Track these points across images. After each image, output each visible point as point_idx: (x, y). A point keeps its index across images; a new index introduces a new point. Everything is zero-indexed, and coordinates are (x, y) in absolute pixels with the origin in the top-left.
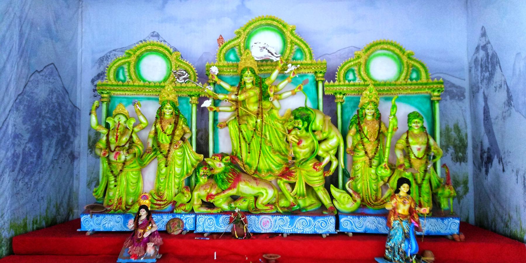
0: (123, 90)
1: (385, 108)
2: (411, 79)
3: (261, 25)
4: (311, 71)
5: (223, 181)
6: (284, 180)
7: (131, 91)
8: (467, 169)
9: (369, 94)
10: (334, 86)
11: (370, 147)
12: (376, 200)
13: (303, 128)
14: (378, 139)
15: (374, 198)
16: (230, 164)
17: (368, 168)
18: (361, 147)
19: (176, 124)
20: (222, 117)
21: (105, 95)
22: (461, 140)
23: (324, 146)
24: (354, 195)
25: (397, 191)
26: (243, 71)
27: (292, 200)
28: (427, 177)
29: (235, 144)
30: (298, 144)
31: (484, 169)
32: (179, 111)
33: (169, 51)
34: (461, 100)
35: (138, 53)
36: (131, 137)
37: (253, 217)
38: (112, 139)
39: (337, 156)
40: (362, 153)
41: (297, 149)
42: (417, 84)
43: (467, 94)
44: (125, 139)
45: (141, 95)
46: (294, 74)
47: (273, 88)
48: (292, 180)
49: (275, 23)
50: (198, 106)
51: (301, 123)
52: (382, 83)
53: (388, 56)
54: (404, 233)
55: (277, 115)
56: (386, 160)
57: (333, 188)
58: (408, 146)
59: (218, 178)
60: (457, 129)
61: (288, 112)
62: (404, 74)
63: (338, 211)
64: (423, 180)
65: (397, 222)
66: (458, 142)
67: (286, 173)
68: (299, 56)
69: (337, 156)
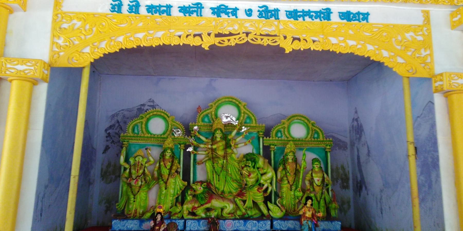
0: (137, 140)
1: (300, 155)
2: (314, 138)
3: (225, 101)
4: (256, 130)
5: (202, 198)
6: (239, 198)
7: (142, 140)
8: (349, 194)
9: (290, 147)
10: (269, 140)
11: (291, 179)
12: (294, 211)
13: (251, 166)
14: (295, 174)
15: (293, 210)
16: (206, 188)
17: (289, 191)
18: (285, 178)
19: (173, 162)
20: (199, 157)
21: (125, 143)
22: (346, 175)
23: (264, 177)
24: (281, 208)
25: (306, 204)
26: (215, 130)
27: (244, 211)
28: (323, 197)
29: (210, 176)
30: (249, 176)
31: (358, 193)
32: (174, 154)
33: (167, 115)
34: (344, 150)
35: (148, 116)
36: (144, 170)
37: (221, 221)
38: (133, 171)
39: (271, 183)
40: (286, 182)
41: (248, 179)
42: (317, 141)
43: (349, 146)
44: (141, 171)
45: (149, 142)
46: (246, 133)
47: (234, 141)
48: (244, 198)
49: (234, 101)
50: (185, 150)
51: (251, 163)
52: (298, 139)
53: (301, 123)
54: (309, 227)
55: (235, 158)
56: (300, 186)
57: (269, 203)
58: (312, 178)
59: (199, 196)
60: (343, 168)
61: (241, 156)
62: (310, 135)
63: (272, 217)
64: (321, 198)
65: (305, 222)
66: (343, 176)
67: (240, 194)
68: (248, 121)
69: (271, 183)
